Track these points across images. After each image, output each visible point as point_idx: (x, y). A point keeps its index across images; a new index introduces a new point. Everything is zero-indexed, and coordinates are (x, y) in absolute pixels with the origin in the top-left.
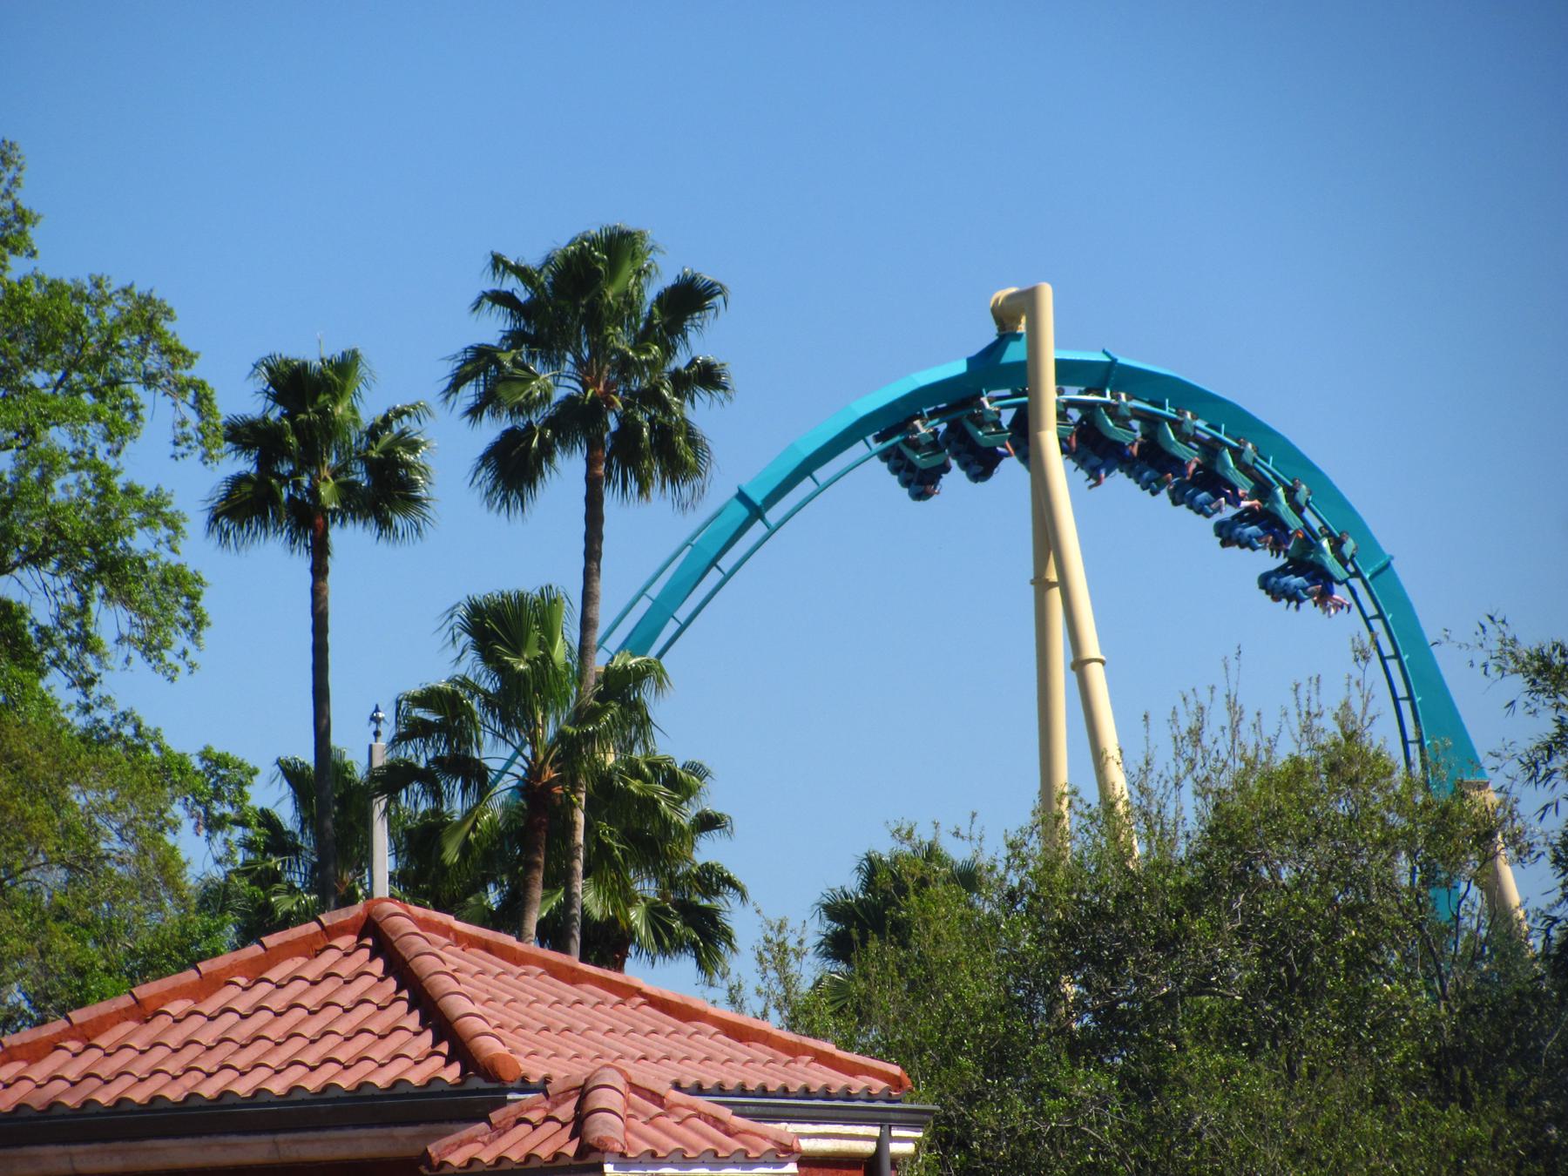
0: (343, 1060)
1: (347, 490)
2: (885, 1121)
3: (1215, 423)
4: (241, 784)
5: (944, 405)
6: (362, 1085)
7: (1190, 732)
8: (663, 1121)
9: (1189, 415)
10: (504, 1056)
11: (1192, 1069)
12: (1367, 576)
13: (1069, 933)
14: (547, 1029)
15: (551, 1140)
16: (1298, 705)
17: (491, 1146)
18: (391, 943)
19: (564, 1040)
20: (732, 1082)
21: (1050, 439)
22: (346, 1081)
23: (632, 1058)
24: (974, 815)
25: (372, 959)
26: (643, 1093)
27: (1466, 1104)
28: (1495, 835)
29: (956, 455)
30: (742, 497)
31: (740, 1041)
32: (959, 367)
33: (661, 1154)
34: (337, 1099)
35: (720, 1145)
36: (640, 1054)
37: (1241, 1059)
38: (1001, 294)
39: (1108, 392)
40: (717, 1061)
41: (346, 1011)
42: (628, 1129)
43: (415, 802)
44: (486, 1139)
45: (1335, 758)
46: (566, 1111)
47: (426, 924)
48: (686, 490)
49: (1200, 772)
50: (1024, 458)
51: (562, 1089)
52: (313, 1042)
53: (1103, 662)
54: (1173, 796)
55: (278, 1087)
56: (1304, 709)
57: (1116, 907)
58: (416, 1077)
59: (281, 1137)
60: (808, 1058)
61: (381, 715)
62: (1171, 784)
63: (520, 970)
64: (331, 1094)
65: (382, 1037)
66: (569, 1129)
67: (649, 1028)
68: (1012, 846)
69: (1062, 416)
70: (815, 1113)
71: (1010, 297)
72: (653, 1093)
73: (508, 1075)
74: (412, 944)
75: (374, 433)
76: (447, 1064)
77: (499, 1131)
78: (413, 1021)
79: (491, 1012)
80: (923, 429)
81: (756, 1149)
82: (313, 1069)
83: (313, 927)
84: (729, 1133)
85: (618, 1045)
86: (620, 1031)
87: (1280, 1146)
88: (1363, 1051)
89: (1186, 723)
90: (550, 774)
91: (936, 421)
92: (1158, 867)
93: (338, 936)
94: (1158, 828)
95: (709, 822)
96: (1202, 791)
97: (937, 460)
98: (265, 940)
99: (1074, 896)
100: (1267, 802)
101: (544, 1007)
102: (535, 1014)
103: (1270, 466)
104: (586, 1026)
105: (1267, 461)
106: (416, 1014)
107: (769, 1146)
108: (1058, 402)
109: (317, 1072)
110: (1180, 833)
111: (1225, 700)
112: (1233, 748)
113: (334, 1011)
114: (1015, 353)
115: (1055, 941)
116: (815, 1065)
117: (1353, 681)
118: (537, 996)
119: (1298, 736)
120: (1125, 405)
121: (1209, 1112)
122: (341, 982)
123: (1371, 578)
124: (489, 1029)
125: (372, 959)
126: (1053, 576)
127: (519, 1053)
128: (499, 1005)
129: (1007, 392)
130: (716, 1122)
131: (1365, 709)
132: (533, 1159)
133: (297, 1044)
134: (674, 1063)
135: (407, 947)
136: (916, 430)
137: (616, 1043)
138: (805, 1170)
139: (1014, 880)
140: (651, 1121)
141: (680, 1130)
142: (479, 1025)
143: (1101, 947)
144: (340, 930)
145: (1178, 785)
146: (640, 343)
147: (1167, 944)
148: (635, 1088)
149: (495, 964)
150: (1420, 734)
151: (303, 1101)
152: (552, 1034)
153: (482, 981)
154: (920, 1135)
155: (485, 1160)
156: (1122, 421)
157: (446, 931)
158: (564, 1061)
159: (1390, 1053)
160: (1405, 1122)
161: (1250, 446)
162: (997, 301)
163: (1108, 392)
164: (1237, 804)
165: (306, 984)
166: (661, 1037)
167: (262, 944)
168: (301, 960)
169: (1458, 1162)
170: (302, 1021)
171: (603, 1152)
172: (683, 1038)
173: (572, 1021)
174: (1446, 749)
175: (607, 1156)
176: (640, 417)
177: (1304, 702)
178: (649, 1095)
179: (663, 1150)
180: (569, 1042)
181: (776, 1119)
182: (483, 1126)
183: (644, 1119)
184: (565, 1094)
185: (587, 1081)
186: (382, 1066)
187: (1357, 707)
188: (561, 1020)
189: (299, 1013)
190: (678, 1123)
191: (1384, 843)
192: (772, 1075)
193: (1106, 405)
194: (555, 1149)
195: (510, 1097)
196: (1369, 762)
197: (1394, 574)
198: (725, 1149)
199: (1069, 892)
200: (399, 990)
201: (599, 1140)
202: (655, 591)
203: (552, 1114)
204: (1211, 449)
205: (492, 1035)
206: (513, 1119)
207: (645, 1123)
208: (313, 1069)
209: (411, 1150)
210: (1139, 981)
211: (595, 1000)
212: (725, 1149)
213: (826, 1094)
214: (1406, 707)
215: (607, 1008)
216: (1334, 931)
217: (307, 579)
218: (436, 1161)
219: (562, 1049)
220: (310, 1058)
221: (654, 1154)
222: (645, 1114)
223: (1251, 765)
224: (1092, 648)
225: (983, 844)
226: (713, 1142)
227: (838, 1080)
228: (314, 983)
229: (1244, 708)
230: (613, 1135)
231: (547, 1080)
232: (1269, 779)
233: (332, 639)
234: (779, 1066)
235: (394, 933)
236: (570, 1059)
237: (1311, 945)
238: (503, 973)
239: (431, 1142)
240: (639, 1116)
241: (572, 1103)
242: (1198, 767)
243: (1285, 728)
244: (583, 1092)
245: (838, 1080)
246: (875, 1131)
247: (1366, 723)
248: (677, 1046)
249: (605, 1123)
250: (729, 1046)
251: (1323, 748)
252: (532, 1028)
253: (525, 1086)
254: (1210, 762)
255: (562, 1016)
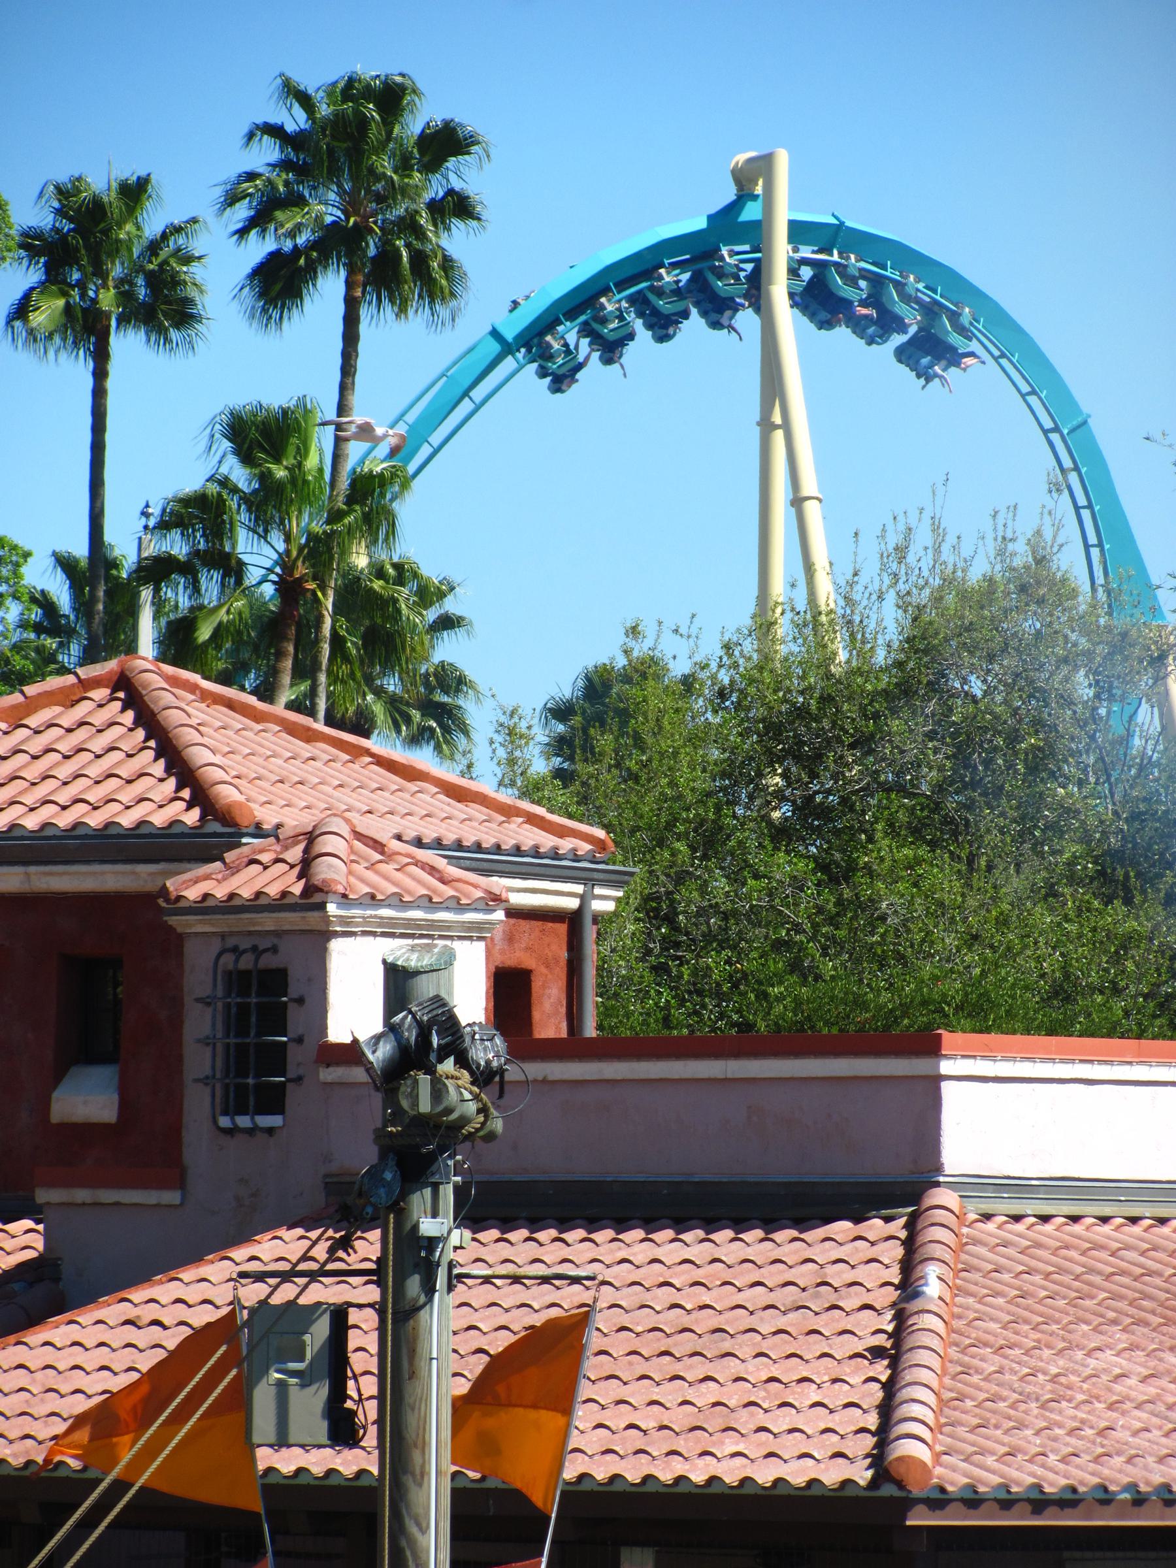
0: (92, 801)
1: (126, 296)
2: (588, 879)
3: (931, 285)
4: (17, 565)
5: (688, 256)
6: (109, 825)
7: (896, 549)
8: (382, 867)
9: (912, 278)
10: (240, 804)
11: (882, 859)
12: (1065, 432)
13: (773, 729)
14: (281, 782)
15: (279, 882)
16: (995, 530)
17: (224, 883)
18: (141, 696)
19: (297, 792)
20: (450, 838)
21: (779, 290)
22: (95, 820)
23: (358, 811)
24: (693, 616)
25: (123, 710)
26: (364, 840)
27: (1128, 901)
28: (1167, 657)
29: (697, 304)
30: (495, 334)
31: (459, 802)
32: (700, 223)
33: (379, 897)
34: (86, 836)
35: (435, 891)
36: (366, 808)
37: (923, 851)
38: (741, 158)
39: (835, 252)
40: (437, 818)
41: (98, 757)
42: (350, 873)
43: (179, 597)
44: (220, 876)
45: (1026, 579)
46: (295, 854)
47: (174, 681)
48: (443, 311)
49: (902, 587)
50: (758, 310)
51: (292, 834)
52: (65, 784)
53: (820, 500)
54: (875, 608)
55: (31, 823)
56: (1000, 534)
57: (819, 709)
58: (159, 819)
59: (32, 869)
60: (521, 820)
61: (150, 510)
62: (874, 597)
63: (259, 727)
64: (80, 831)
65: (129, 782)
66: (297, 870)
67: (376, 785)
68: (727, 647)
69: (793, 272)
70: (524, 869)
71: (750, 161)
72: (376, 841)
73: (244, 821)
74: (159, 698)
75: (154, 247)
76: (189, 808)
77: (232, 870)
78: (159, 768)
79: (230, 763)
80: (667, 277)
81: (467, 896)
82: (64, 808)
83: (70, 679)
84: (443, 881)
85: (346, 798)
86: (349, 786)
87: (957, 932)
88: (1037, 845)
89: (893, 540)
90: (301, 570)
91: (677, 271)
92: (859, 672)
93: (94, 689)
94: (859, 636)
95: (448, 623)
96: (903, 606)
97: (679, 306)
98: (25, 689)
99: (781, 694)
100: (962, 617)
101: (280, 762)
102: (271, 767)
103: (980, 327)
104: (318, 780)
105: (978, 322)
106: (162, 763)
107: (479, 894)
108: (790, 259)
109: (67, 811)
110: (880, 641)
111: (930, 522)
112: (934, 566)
113: (86, 757)
114: (751, 212)
115: (759, 735)
116: (527, 826)
117: (1046, 511)
118: (274, 751)
119: (992, 559)
120: (854, 266)
121: (894, 899)
122: (94, 730)
123: (1071, 432)
124: (228, 779)
125: (123, 710)
126: (777, 418)
127: (254, 802)
128: (238, 758)
129: (747, 247)
130: (432, 870)
131: (1054, 537)
132: (262, 896)
133: (51, 784)
134: (397, 818)
135: (156, 702)
136: (661, 278)
137: (344, 798)
138: (512, 921)
139: (724, 677)
140: (372, 867)
141: (399, 876)
142: (218, 774)
143: (802, 743)
144: (95, 683)
145: (881, 598)
146: (404, 165)
147: (864, 743)
148: (359, 836)
149: (237, 721)
150: (1107, 582)
151: (54, 837)
152: (286, 786)
153: (224, 736)
154: (620, 894)
155: (218, 896)
156: (852, 281)
157: (192, 688)
158: (296, 811)
159: (1060, 852)
160: (1072, 914)
161: (967, 310)
162: (737, 163)
163: (835, 252)
164: (930, 615)
165: (62, 731)
166: (386, 794)
167: (22, 692)
168: (58, 709)
169: (1117, 952)
170: (57, 765)
171: (327, 893)
172: (407, 796)
173: (305, 775)
174: (1129, 577)
175: (331, 897)
176: (400, 243)
177: (1000, 528)
178: (371, 843)
179: (382, 893)
180: (302, 795)
181: (487, 873)
182: (218, 864)
183: (366, 865)
184: (295, 839)
185: (315, 827)
186: (128, 808)
187: (1048, 534)
188: (294, 774)
189: (54, 757)
190: (398, 870)
191: (1065, 660)
192: (487, 833)
193: (836, 264)
194: (282, 888)
195: (244, 840)
196: (1055, 585)
197: (1090, 432)
198: (439, 895)
199: (775, 691)
200: (147, 739)
201: (324, 881)
202: (411, 417)
203: (281, 856)
204: (931, 311)
205: (230, 784)
206: (246, 860)
207: (367, 868)
208: (64, 808)
209: (151, 886)
210: (835, 777)
211: (327, 757)
212: (439, 895)
213: (536, 852)
214: (1095, 553)
215: (338, 765)
216: (1013, 738)
217: (89, 382)
218: (173, 895)
219: (295, 800)
220: (63, 797)
221: (373, 897)
222: (367, 860)
223: (948, 582)
224: (809, 486)
225: (699, 642)
226: (429, 888)
227: (547, 841)
228: (69, 730)
229: (948, 530)
230: (336, 877)
231: (279, 826)
232: (964, 595)
233: (109, 437)
234: (494, 826)
235: (144, 688)
236: (301, 810)
237: (996, 749)
238: (243, 729)
239: (168, 879)
240: (361, 861)
241: (301, 847)
242: (901, 581)
243: (981, 551)
244: (311, 837)
245: (547, 841)
246: (579, 889)
247: (1055, 549)
248: (401, 802)
249: (330, 866)
250: (449, 805)
251: (1014, 569)
252: (268, 780)
253: (259, 831)
254: (913, 578)
255: (296, 770)
